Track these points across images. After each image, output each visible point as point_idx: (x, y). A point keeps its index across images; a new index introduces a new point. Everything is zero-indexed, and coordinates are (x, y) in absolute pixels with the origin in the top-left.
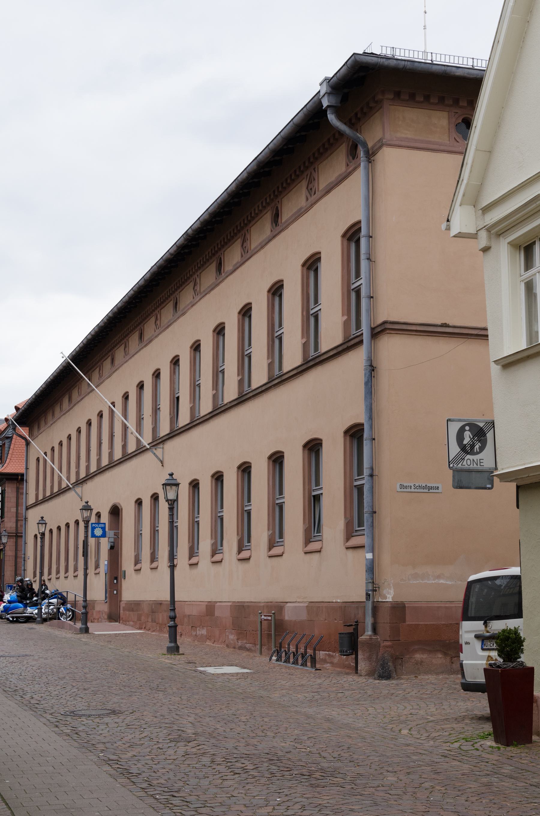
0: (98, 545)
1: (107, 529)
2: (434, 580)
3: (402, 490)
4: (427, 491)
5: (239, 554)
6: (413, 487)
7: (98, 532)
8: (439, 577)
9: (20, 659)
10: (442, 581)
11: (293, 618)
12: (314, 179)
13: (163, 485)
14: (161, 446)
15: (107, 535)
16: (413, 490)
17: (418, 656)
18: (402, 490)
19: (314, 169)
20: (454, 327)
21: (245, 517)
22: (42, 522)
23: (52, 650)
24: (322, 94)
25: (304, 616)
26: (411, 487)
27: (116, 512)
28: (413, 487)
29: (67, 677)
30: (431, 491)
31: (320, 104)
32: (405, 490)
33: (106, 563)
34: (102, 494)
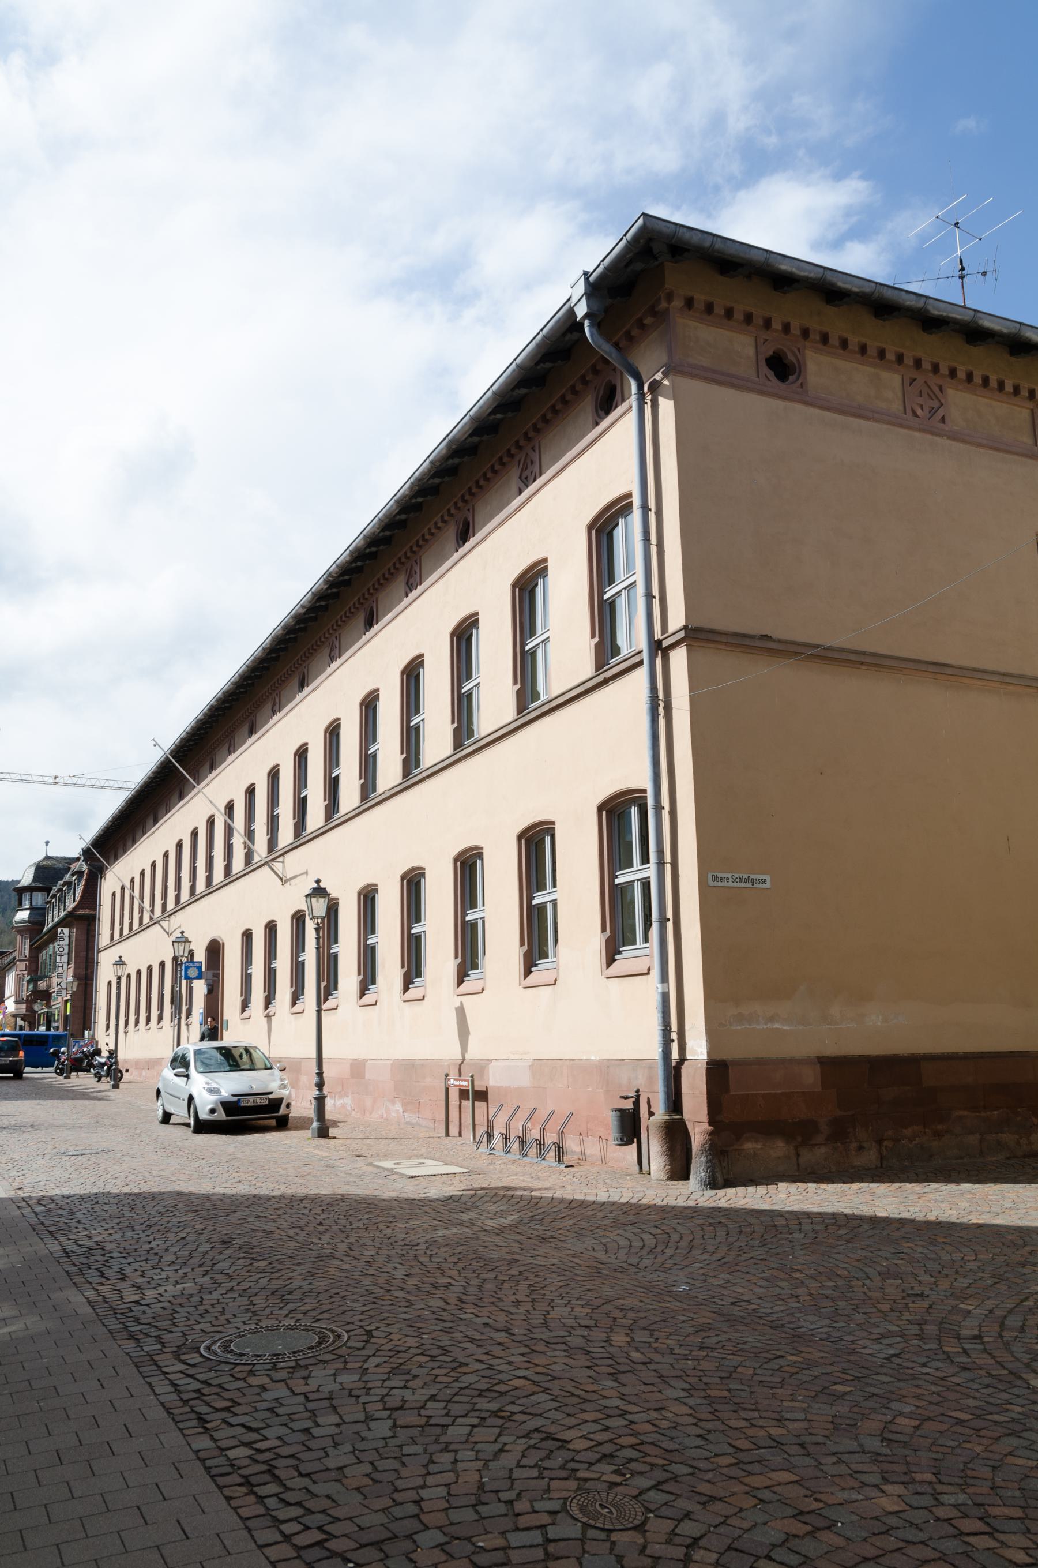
0: (190, 990)
1: (203, 969)
2: (766, 1024)
3: (716, 884)
4: (750, 885)
5: (361, 998)
6: (731, 880)
7: (193, 972)
8: (772, 1019)
9: (93, 1159)
10: (776, 1026)
11: (505, 1083)
12: (532, 462)
13: (306, 896)
14: (280, 859)
15: (204, 975)
16: (730, 884)
17: (749, 1146)
18: (716, 884)
19: (533, 449)
20: (780, 641)
21: (270, 975)
22: (120, 962)
23: (139, 1135)
24: (574, 300)
25: (524, 1080)
26: (728, 879)
27: (215, 950)
28: (731, 880)
29: (180, 1206)
30: (756, 886)
31: (571, 312)
32: (720, 884)
33: (202, 1011)
34: (206, 922)
